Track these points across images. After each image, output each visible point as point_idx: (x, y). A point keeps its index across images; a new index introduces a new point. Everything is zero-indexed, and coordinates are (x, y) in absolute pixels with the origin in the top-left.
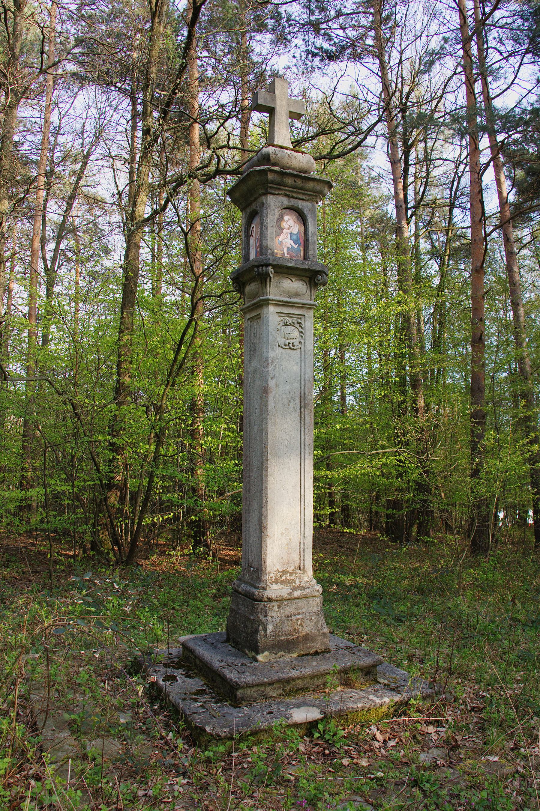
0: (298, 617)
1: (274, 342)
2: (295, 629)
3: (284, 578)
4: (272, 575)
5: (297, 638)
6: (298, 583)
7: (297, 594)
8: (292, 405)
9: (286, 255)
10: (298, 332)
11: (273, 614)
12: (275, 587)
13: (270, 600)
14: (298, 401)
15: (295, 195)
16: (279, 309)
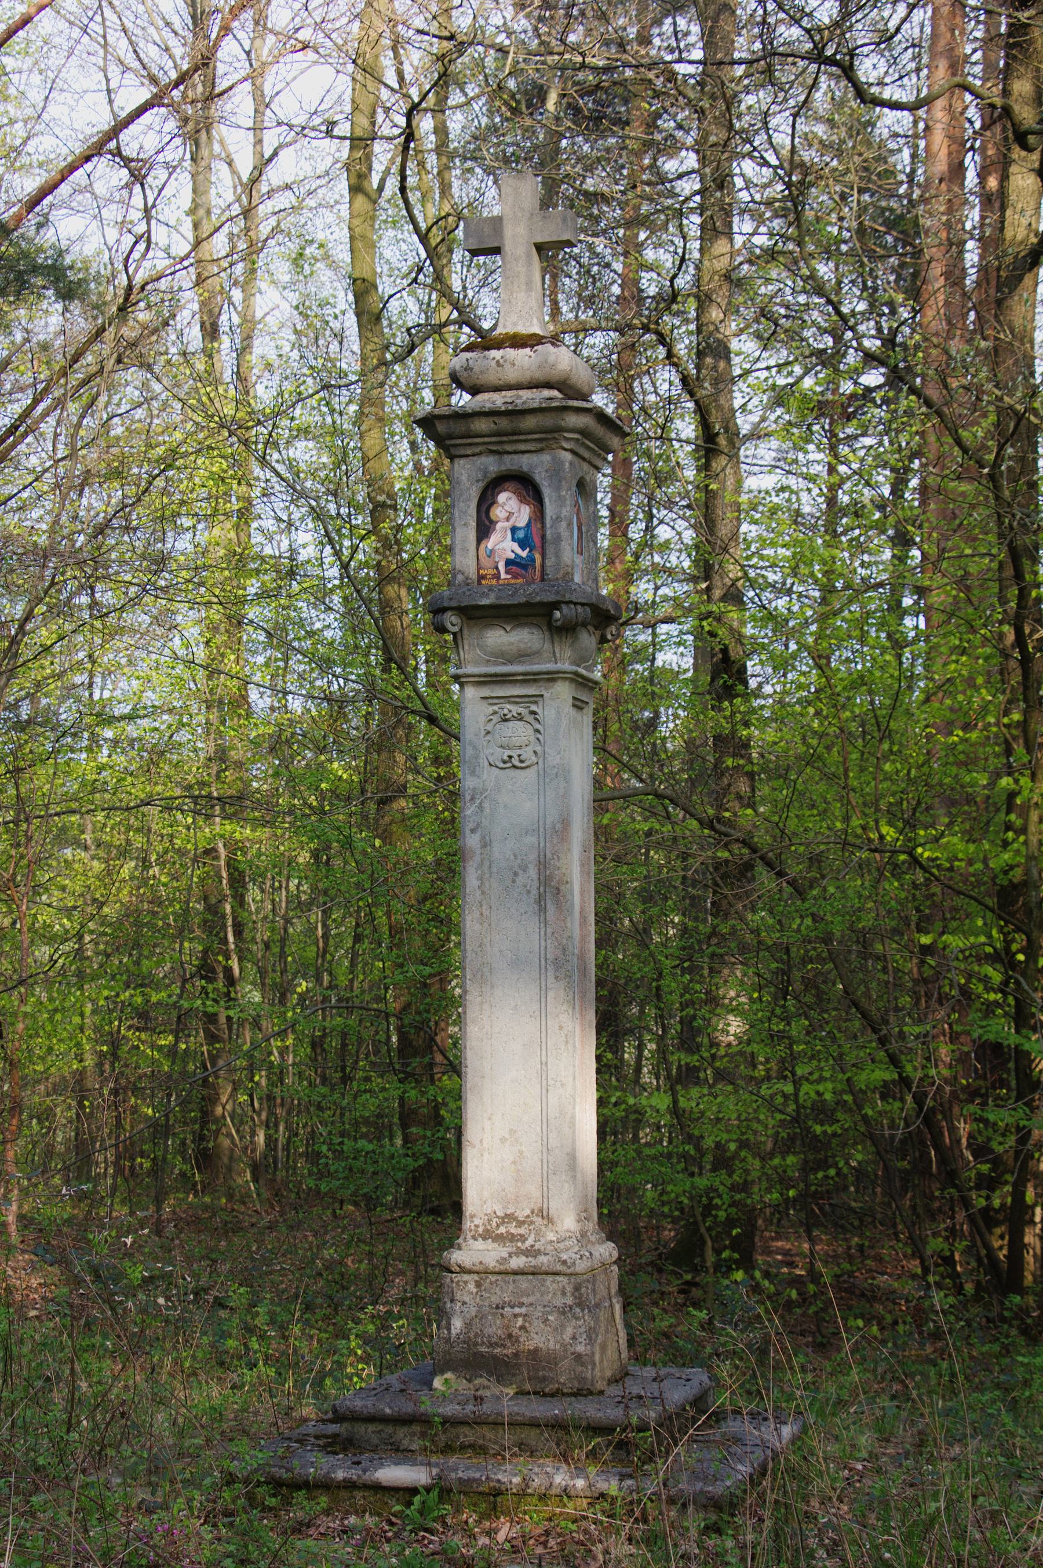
0: (517, 1310)
1: (477, 757)
2: (510, 1336)
3: (502, 1230)
4: (477, 1221)
5: (516, 1355)
6: (530, 1242)
7: (518, 1263)
8: (521, 880)
9: (503, 576)
10: (531, 732)
11: (467, 1299)
12: (480, 1244)
13: (463, 1270)
14: (533, 872)
15: (508, 448)
16: (486, 692)
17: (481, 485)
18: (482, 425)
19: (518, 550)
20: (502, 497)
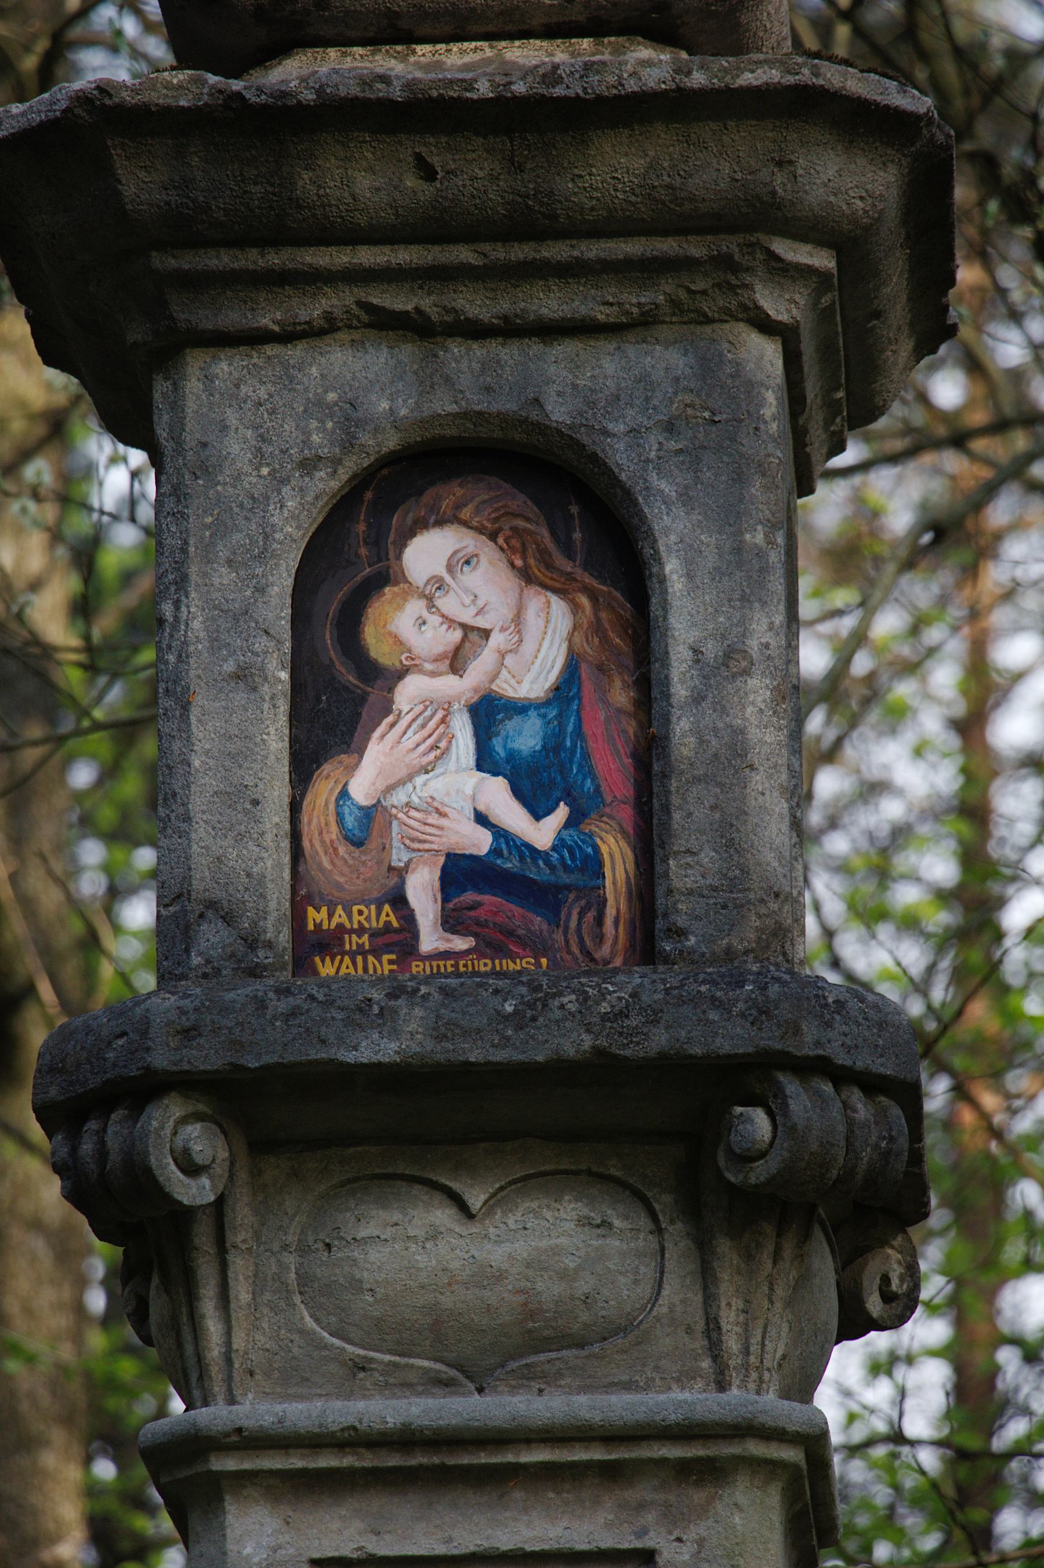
9: (431, 938)
15: (474, 303)
17: (327, 484)
18: (364, 180)
19: (514, 817)
20: (426, 553)
